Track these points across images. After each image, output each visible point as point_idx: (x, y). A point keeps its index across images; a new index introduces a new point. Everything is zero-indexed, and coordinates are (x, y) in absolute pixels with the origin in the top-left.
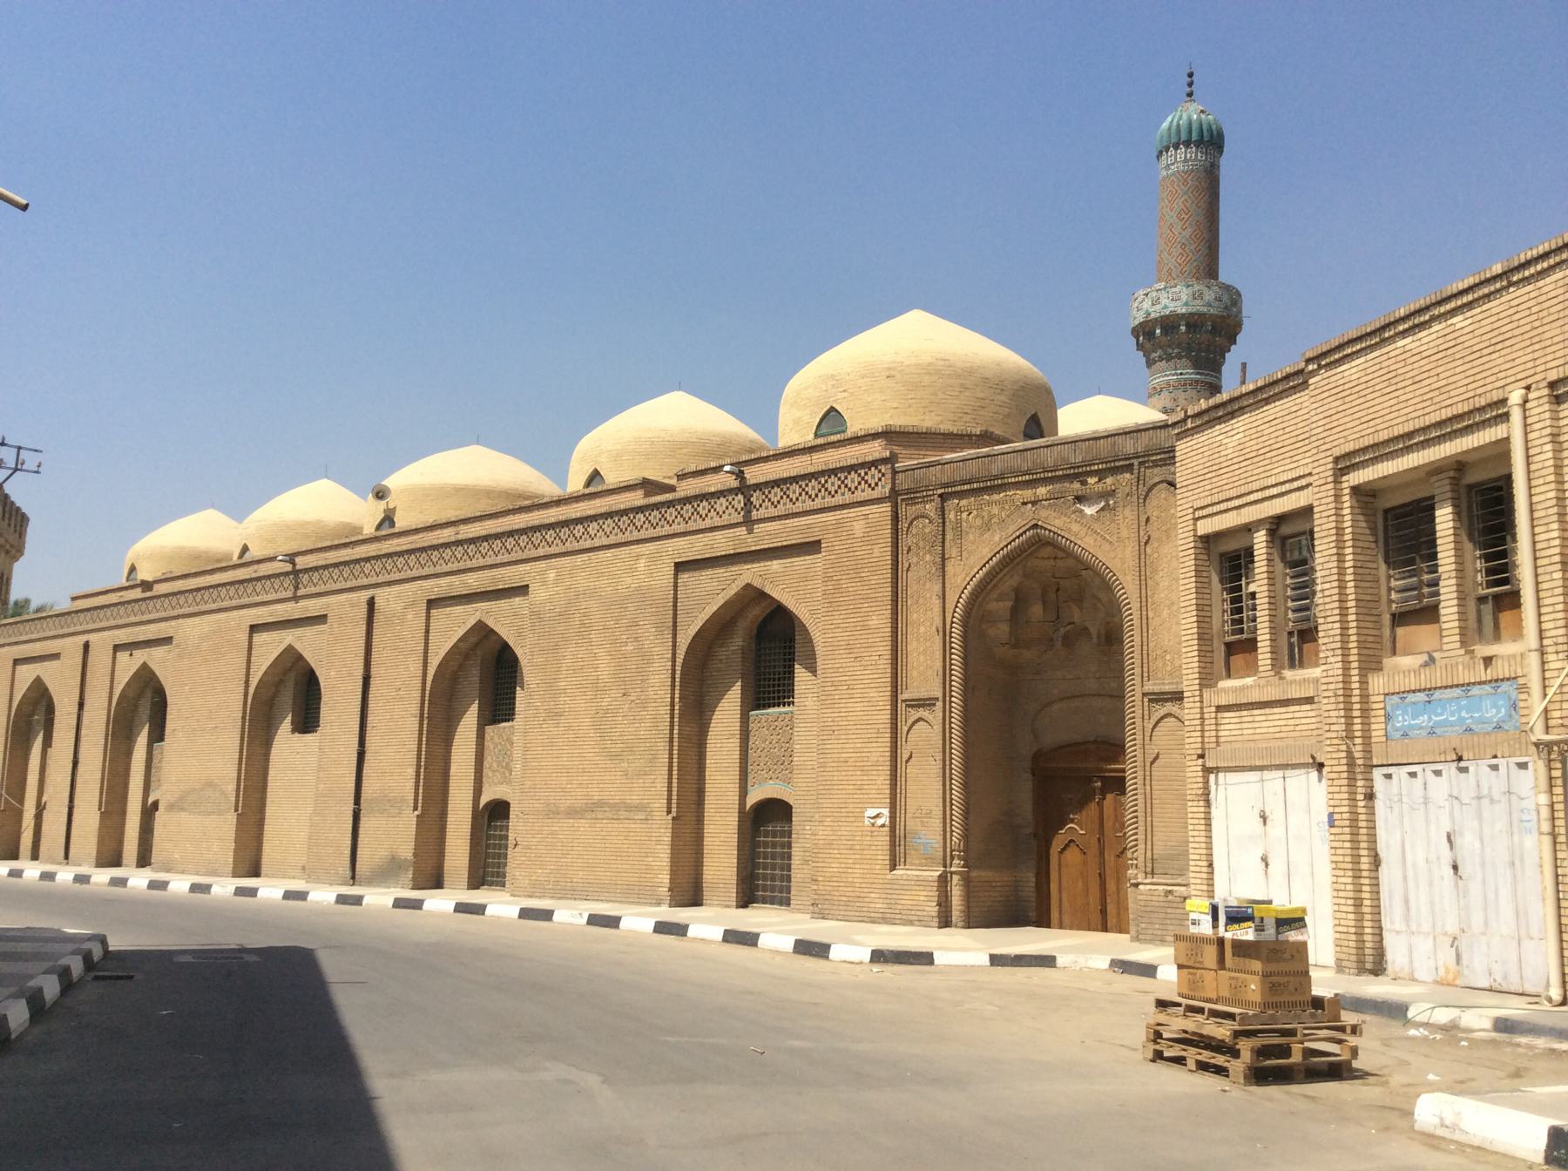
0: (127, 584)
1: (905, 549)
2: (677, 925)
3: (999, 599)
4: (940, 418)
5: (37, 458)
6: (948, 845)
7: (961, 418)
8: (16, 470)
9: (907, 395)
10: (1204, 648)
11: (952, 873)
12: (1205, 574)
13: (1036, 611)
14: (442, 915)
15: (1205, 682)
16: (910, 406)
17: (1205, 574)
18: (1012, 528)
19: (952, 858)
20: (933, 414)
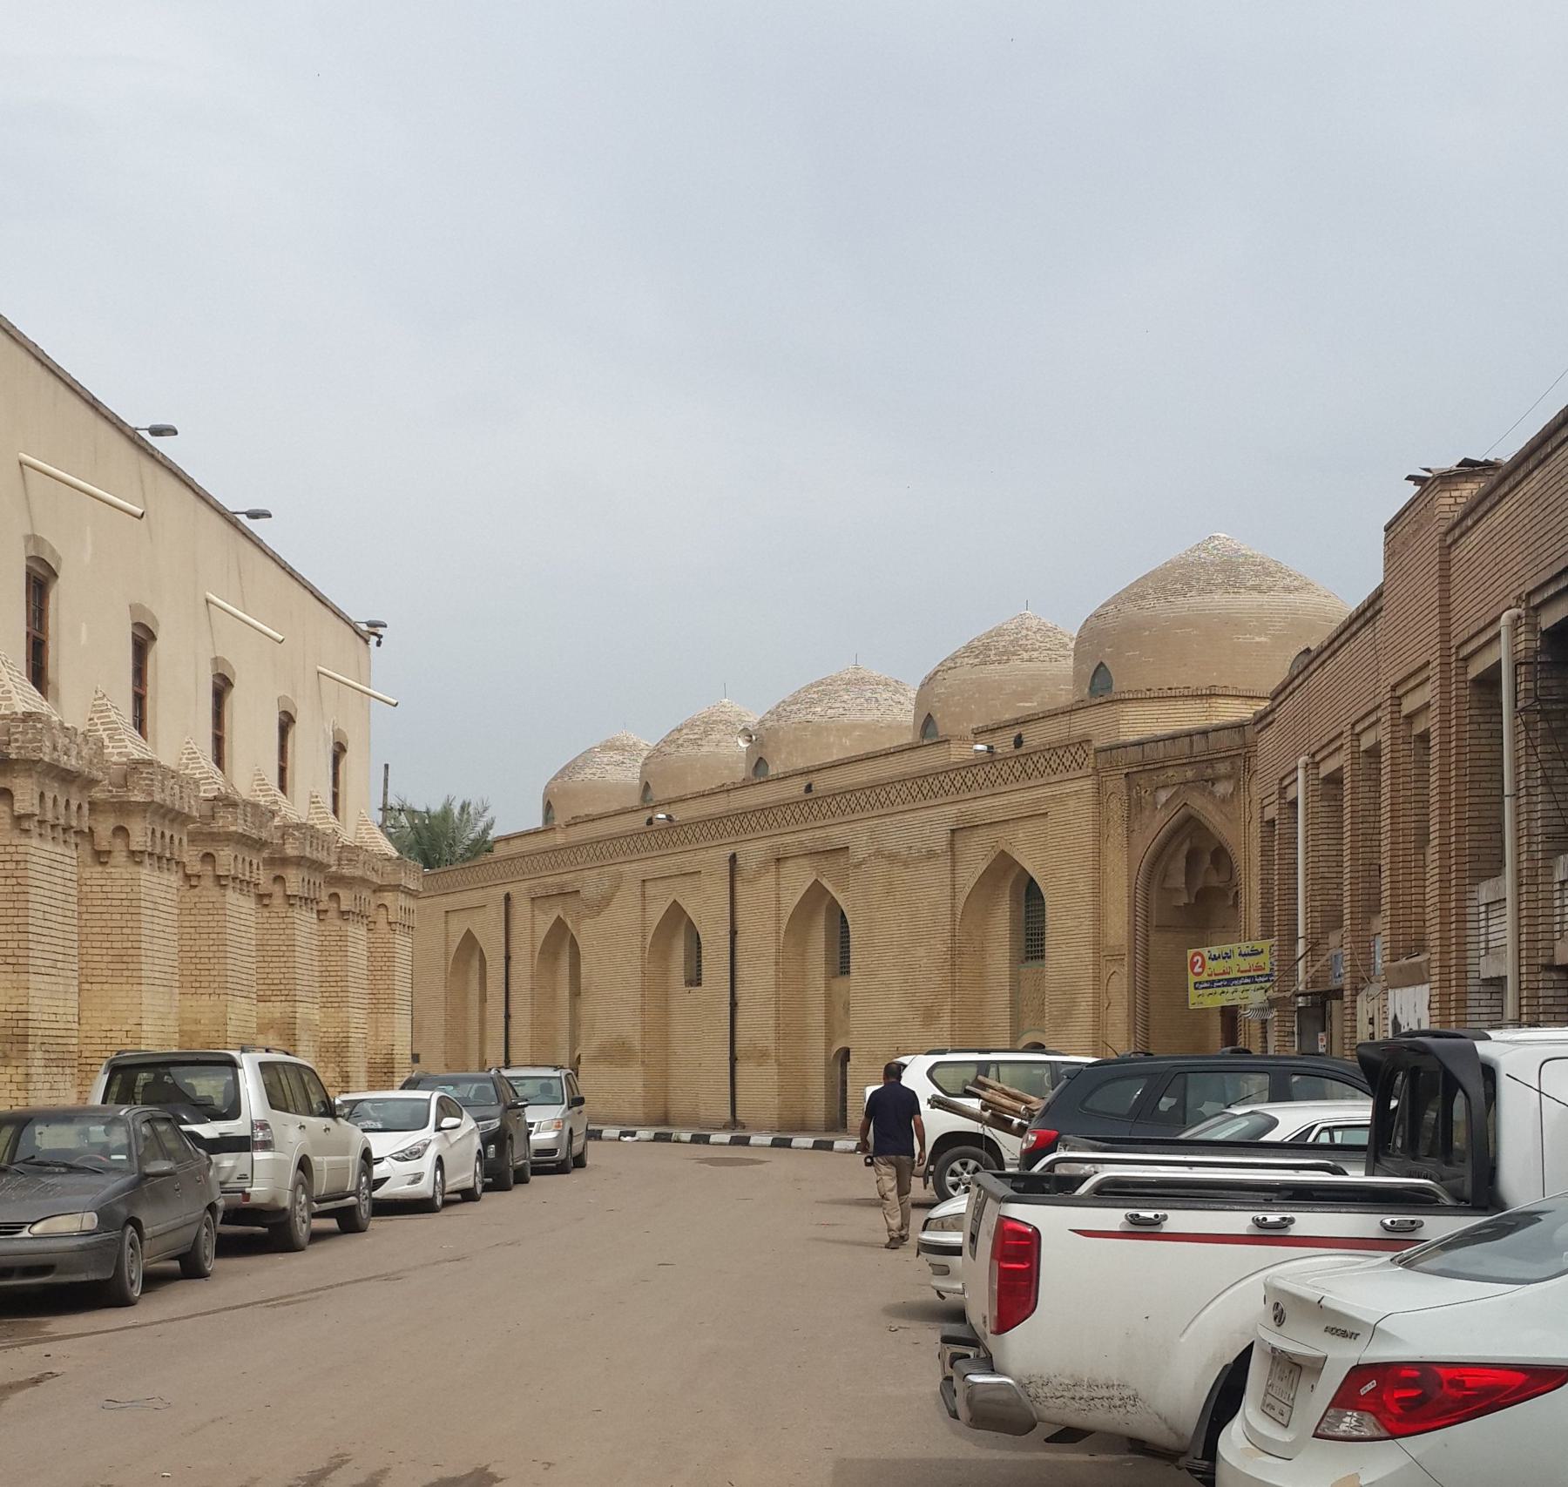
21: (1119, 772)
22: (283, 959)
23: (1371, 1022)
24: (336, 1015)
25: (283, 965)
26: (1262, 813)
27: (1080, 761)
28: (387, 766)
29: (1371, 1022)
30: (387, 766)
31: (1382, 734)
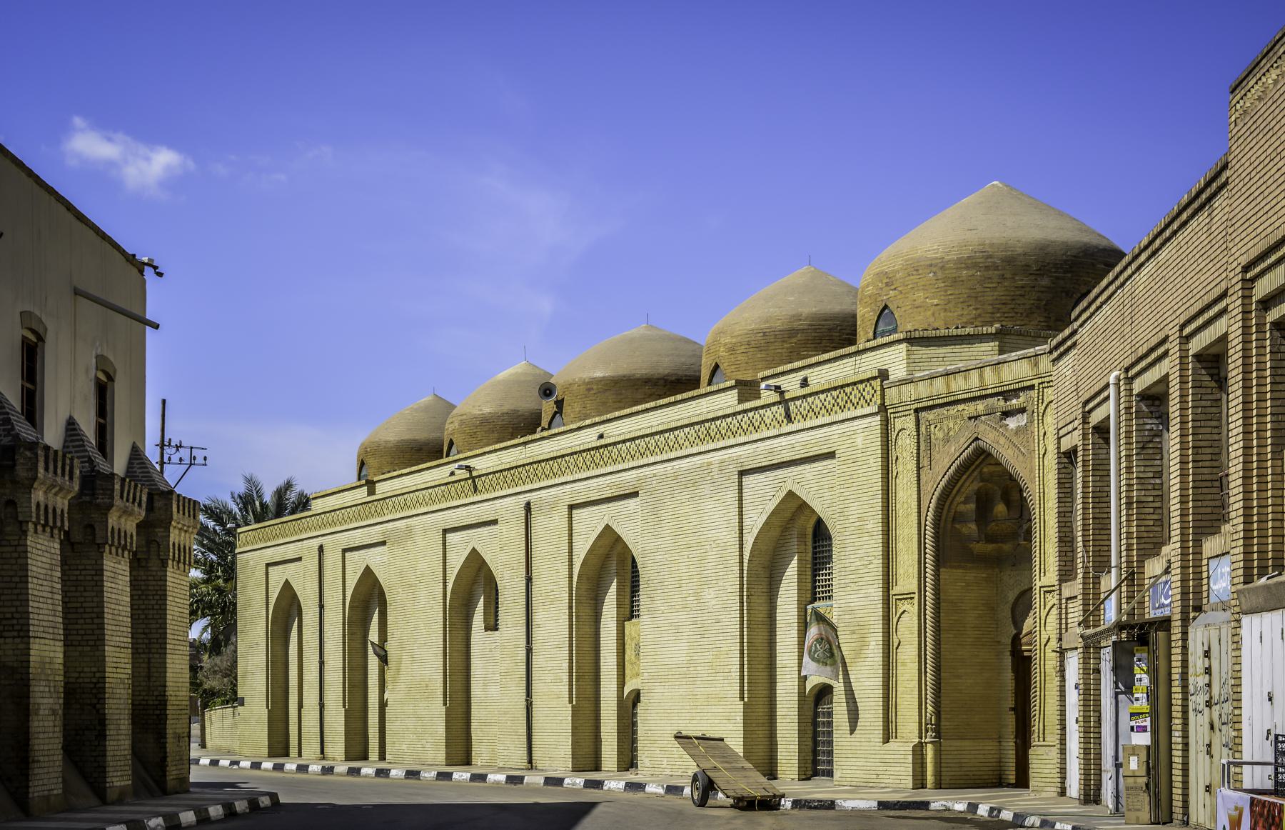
0: (358, 484)
1: (894, 458)
2: (482, 775)
3: (965, 502)
4: (979, 311)
5: (204, 453)
6: (923, 720)
7: (999, 309)
8: (191, 464)
9: (946, 291)
10: (1064, 549)
11: (926, 743)
12: (1067, 485)
13: (1000, 508)
14: (658, 795)
15: (1064, 578)
16: (949, 302)
17: (1067, 485)
18: (963, 440)
19: (927, 731)
20: (971, 308)
21: (908, 407)
22: (16, 591)
23: (1207, 654)
24: (92, 654)
25: (15, 597)
26: (1059, 443)
27: (868, 398)
28: (164, 401)
29: (1207, 654)
30: (164, 401)
31: (1229, 325)
